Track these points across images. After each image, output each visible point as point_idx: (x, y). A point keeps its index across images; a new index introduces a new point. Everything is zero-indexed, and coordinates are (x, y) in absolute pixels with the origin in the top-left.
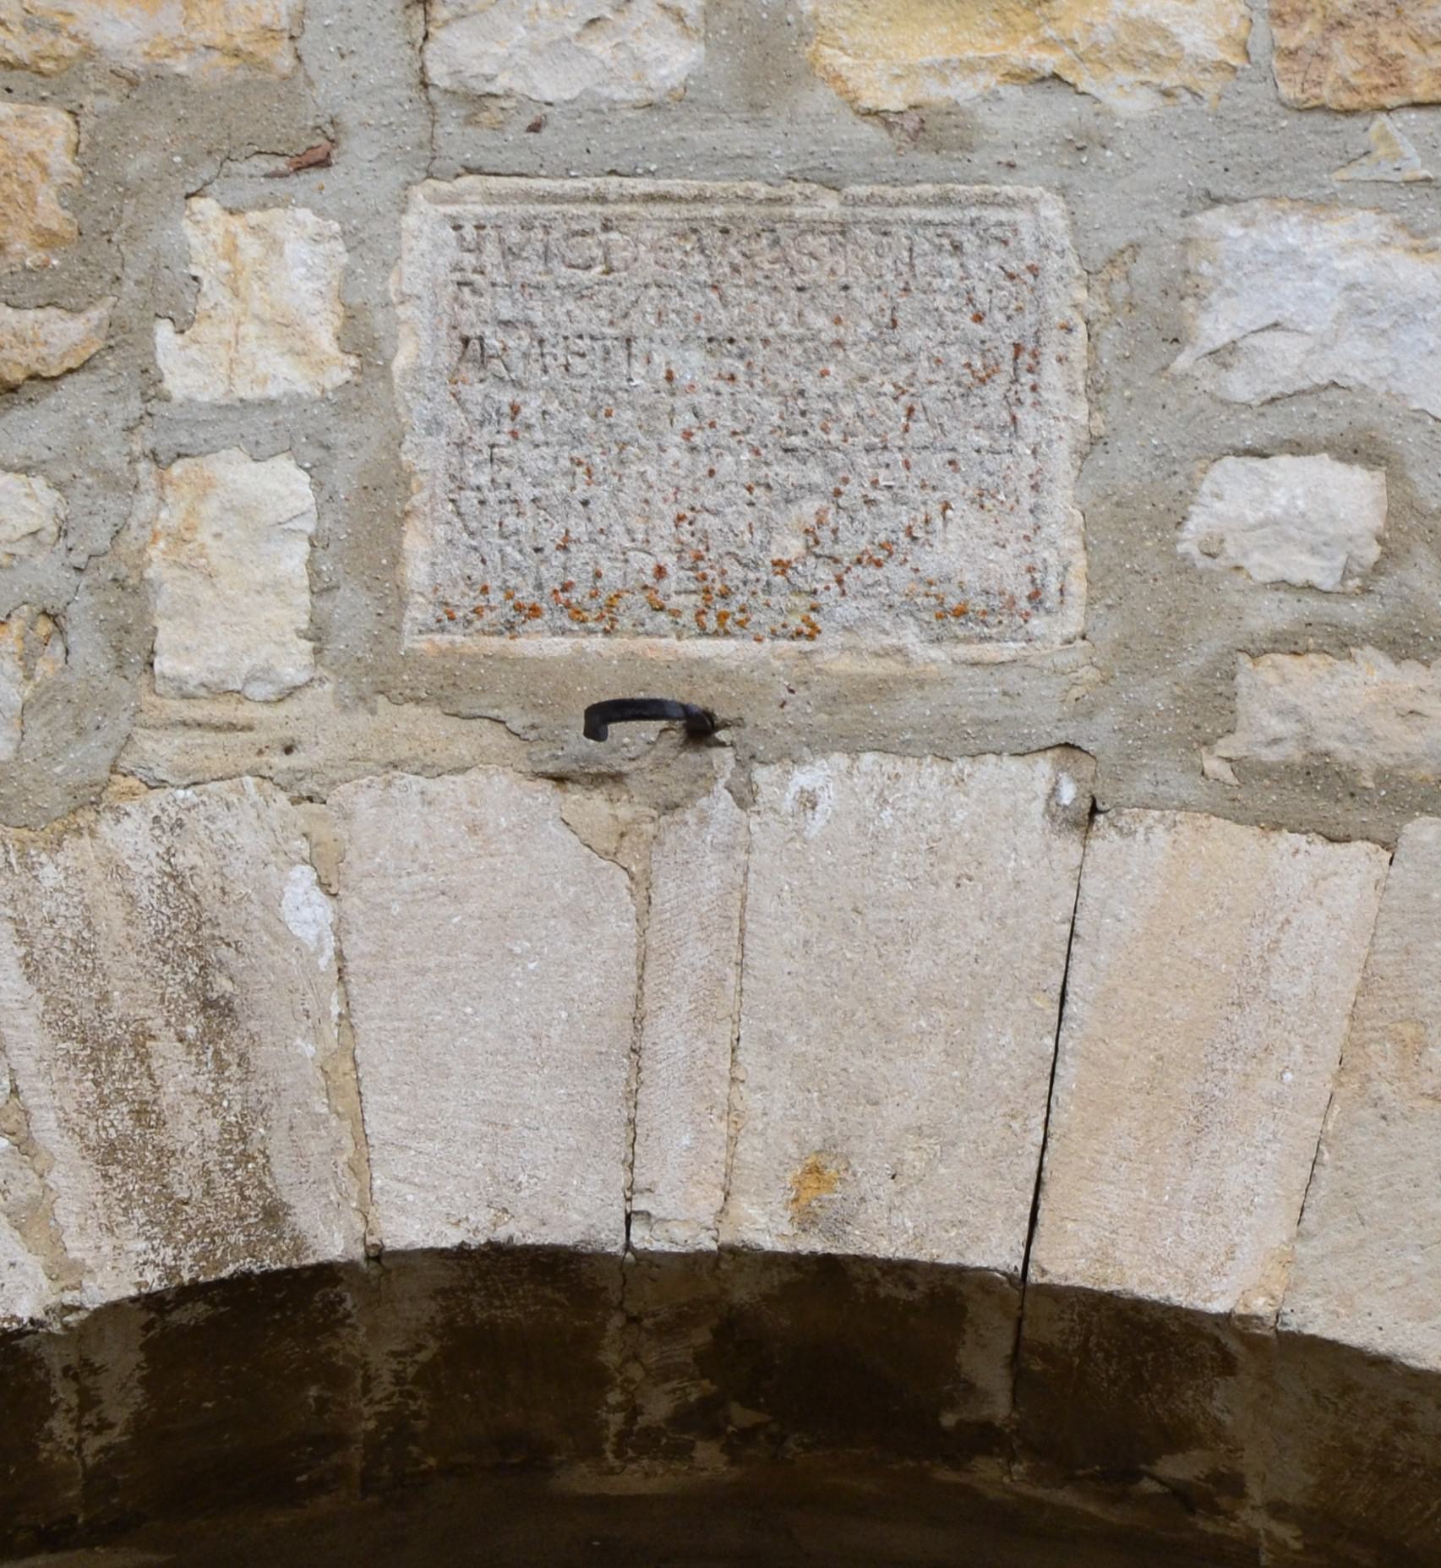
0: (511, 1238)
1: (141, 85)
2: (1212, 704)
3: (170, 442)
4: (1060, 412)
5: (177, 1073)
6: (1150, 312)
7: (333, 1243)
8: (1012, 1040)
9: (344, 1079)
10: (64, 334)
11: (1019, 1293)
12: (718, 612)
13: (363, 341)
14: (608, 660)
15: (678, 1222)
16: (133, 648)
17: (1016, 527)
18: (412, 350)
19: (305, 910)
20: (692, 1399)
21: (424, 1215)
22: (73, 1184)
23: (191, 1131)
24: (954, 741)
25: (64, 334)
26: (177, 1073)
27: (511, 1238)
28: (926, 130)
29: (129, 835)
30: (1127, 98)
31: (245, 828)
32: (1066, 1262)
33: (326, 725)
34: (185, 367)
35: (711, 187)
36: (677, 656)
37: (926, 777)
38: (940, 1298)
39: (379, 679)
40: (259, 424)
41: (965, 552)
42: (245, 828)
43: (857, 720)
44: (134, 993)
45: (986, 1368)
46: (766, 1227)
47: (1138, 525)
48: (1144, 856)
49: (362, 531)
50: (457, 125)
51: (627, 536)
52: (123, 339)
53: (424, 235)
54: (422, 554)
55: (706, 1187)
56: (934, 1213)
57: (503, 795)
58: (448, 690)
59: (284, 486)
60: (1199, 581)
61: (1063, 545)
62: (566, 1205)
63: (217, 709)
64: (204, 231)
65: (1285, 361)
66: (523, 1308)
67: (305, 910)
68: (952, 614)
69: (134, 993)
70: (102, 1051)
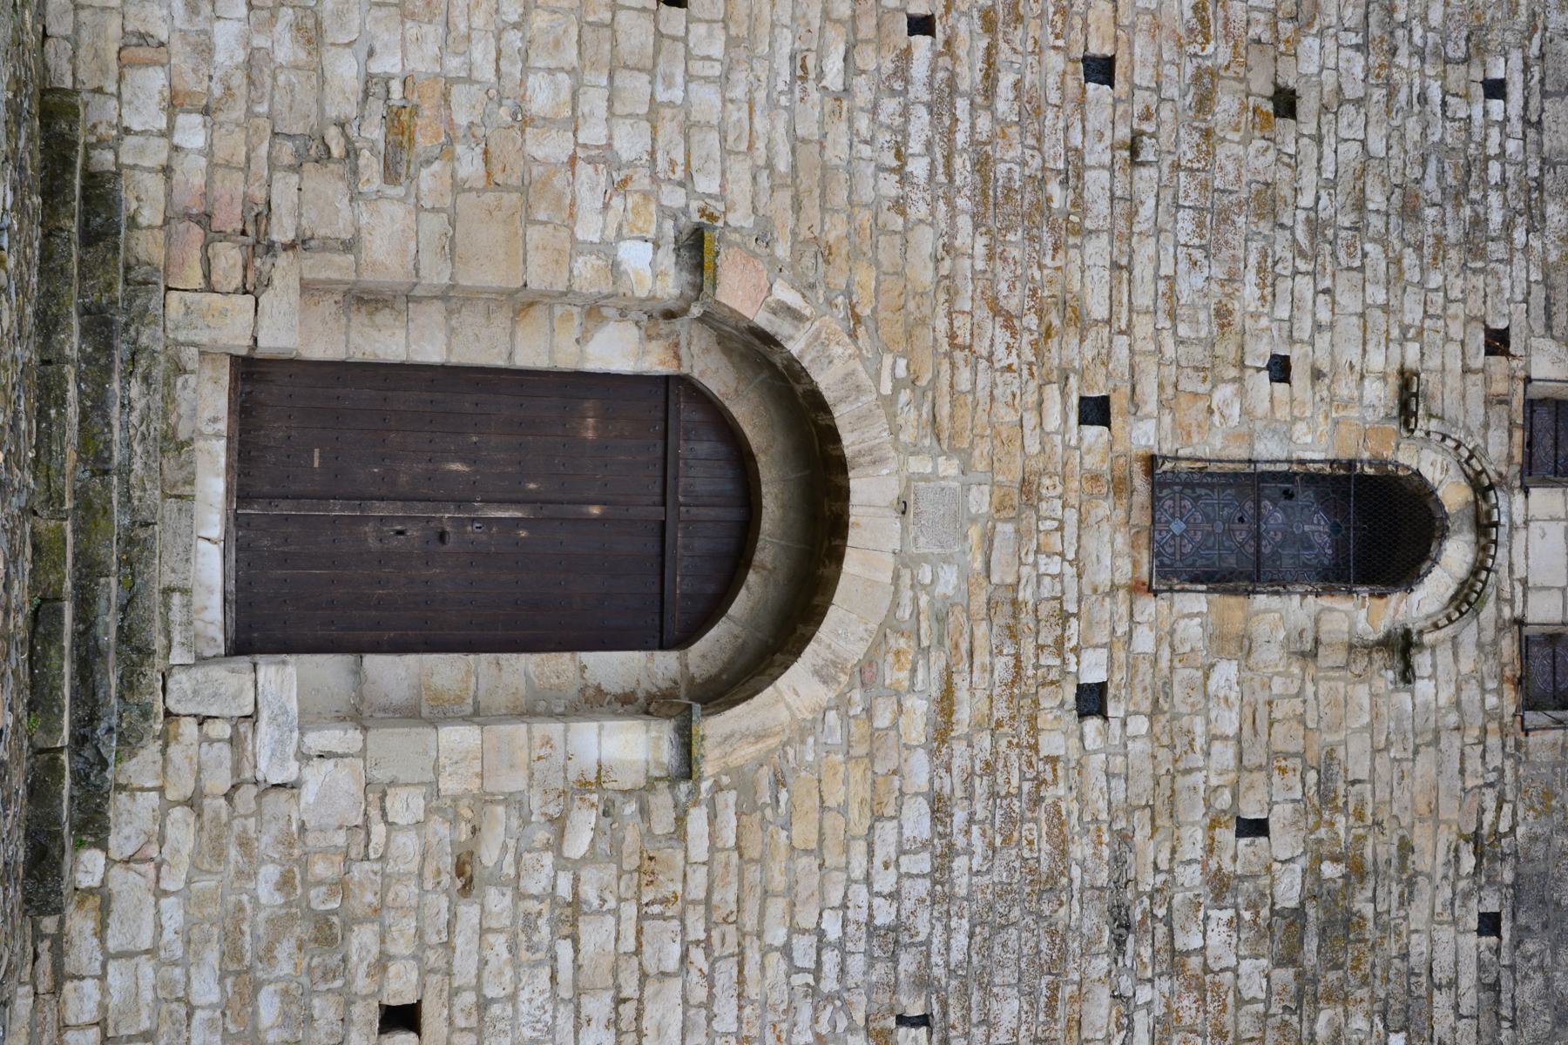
0: (707, 350)
1: (971, 455)
2: (905, 566)
3: (934, 458)
4: (937, 551)
5: (868, 458)
6: (947, 560)
7: (850, 475)
8: (871, 545)
9: (868, 475)
10: (945, 447)
11: (845, 545)
12: (916, 515)
13: (944, 478)
14: (911, 503)
15: (852, 511)
16: (912, 454)
17: (924, 546)
18: (943, 483)
19: (885, 472)
20: (696, 416)
21: (854, 484)
22: (856, 448)
23: (862, 460)
24: (902, 539)
25: (945, 447)
26: (868, 458)
27: (707, 350)
28: (966, 537)
29: (893, 453)
30: (969, 558)
31: (893, 465)
32: (848, 550)
33: (904, 474)
34: (941, 459)
35: (989, 335)
36: (911, 510)
37: (898, 536)
38: (845, 537)
39: (909, 479)
40: (935, 467)
41: (922, 540)
42: (893, 465)
43: (904, 529)
44: (876, 454)
45: (837, 542)
46: (852, 519)
47: (924, 558)
48: (890, 559)
49: (925, 478)
50: (967, 488)
51: (923, 505)
52: (944, 453)
53: (956, 484)
54: (922, 484)
55: (856, 513)
56: (853, 535)
57: (897, 492)
58: (908, 487)
59: (929, 470)
60: (918, 564)
61: (922, 551)
62: (854, 498)
63: (905, 462)
64: (956, 462)
65: (941, 574)
66: (843, 494)
67: (885, 472)
68: (915, 539)
69: (876, 454)
70: (871, 451)
